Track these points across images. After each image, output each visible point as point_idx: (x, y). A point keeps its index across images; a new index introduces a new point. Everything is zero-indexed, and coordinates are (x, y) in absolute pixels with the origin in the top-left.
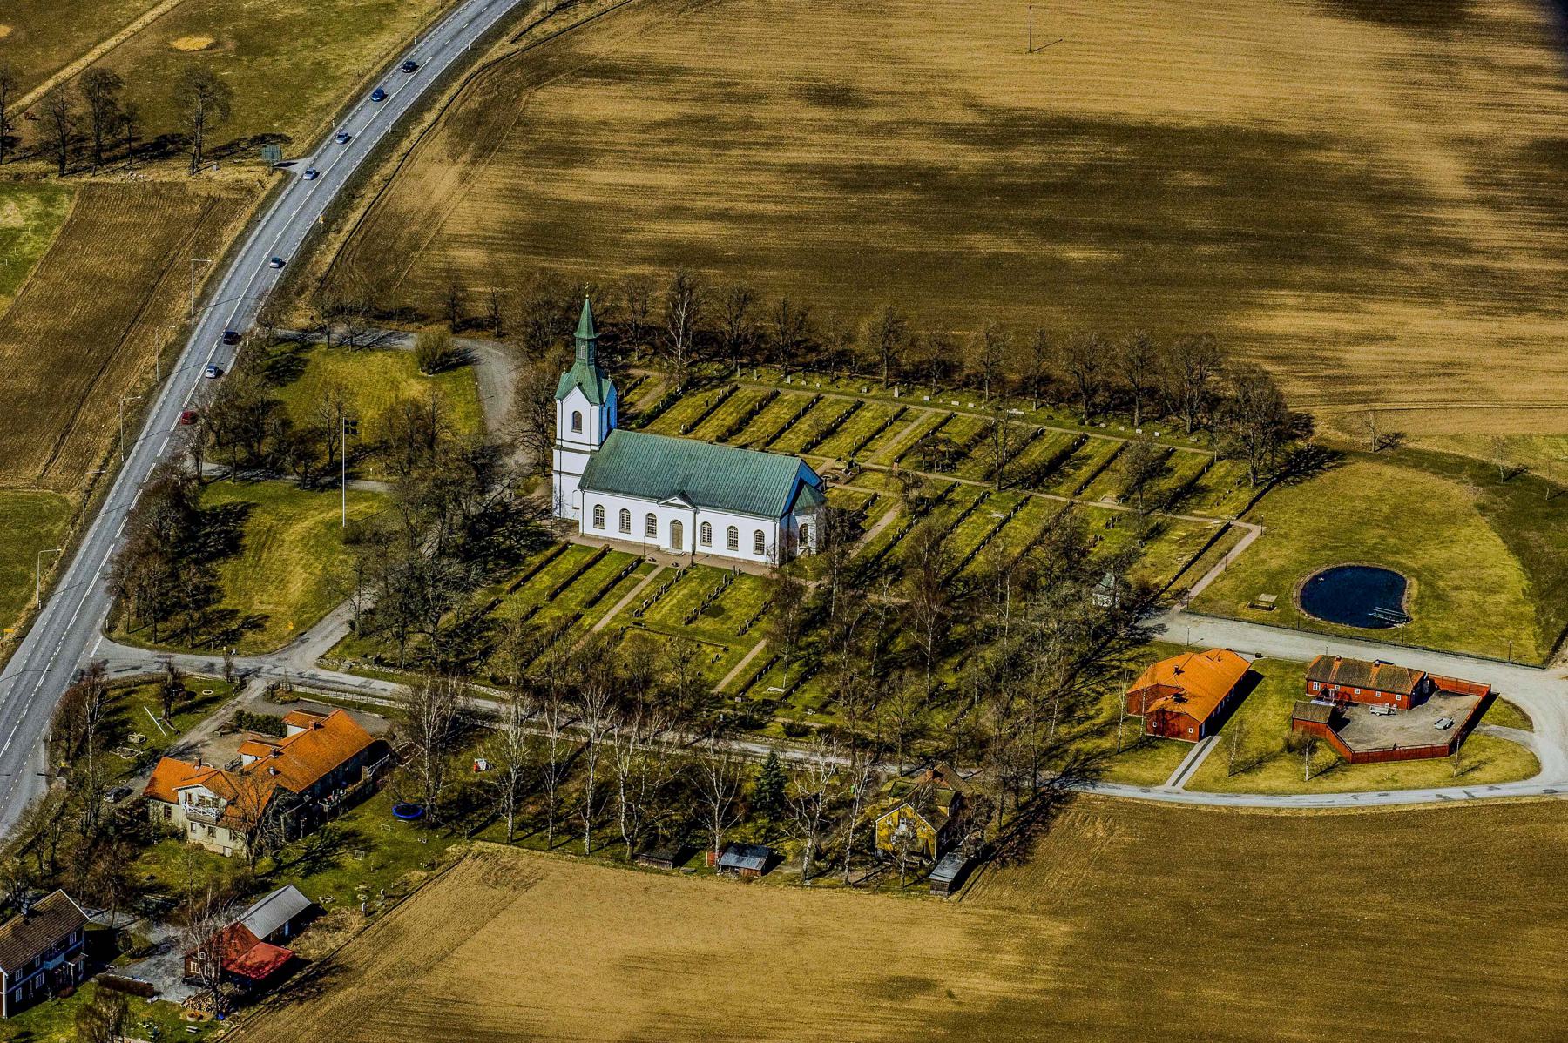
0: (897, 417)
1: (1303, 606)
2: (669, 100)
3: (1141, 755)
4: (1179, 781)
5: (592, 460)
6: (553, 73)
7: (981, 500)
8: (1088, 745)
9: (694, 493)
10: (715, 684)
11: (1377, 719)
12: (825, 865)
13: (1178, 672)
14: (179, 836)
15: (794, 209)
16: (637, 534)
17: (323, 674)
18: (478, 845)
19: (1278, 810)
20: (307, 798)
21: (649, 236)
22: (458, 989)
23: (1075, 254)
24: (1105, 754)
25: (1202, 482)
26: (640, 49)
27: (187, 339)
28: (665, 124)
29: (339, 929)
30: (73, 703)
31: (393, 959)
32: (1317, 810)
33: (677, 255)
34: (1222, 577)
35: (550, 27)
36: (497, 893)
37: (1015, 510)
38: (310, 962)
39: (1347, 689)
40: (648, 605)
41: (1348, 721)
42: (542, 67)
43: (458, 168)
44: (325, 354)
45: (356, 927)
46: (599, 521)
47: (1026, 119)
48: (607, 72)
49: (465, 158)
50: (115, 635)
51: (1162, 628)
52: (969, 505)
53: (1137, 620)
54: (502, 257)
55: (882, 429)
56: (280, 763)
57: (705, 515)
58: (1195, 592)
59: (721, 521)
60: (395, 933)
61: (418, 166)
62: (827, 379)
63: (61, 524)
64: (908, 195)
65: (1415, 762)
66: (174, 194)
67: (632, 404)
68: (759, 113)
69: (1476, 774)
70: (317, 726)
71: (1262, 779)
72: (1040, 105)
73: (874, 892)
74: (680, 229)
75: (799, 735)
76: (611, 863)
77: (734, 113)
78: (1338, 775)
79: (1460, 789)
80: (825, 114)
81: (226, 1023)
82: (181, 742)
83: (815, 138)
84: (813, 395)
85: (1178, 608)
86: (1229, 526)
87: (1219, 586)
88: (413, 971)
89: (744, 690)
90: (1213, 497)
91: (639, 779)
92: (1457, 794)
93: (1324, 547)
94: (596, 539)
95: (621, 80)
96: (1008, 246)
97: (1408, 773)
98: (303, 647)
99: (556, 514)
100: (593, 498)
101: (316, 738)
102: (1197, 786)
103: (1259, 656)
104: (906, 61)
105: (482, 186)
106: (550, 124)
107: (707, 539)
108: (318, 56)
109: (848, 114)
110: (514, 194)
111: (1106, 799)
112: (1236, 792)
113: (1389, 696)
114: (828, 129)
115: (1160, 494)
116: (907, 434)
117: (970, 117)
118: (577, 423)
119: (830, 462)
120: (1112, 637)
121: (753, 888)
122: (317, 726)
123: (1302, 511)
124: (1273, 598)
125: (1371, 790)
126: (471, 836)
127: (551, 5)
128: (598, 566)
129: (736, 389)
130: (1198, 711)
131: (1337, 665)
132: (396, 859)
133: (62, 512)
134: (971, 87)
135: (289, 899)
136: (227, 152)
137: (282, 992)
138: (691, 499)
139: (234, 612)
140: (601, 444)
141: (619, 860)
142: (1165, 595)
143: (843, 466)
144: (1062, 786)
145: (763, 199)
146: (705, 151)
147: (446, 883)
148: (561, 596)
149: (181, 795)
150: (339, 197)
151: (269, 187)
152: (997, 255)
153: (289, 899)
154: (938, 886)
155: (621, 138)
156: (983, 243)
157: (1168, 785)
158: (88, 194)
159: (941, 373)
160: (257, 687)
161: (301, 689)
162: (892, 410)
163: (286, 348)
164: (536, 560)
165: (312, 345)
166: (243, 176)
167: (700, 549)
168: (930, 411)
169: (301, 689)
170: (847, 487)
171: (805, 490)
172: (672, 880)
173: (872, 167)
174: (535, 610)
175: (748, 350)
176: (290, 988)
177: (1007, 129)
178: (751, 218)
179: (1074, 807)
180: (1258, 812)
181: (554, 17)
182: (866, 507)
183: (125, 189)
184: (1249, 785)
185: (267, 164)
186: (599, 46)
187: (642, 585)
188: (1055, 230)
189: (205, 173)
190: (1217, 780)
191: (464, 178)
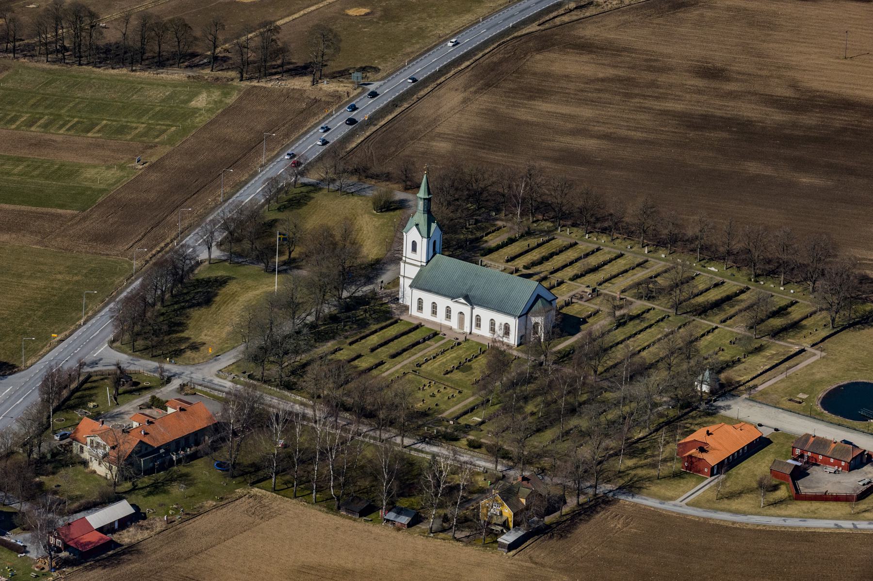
0: (639, 265)
1: (821, 403)
2: (613, 66)
3: (675, 482)
4: (685, 501)
5: (420, 271)
6: (553, 45)
7: (662, 320)
8: (641, 472)
9: (474, 297)
10: (443, 411)
11: (827, 475)
12: (444, 527)
13: (709, 434)
14: (85, 463)
15: (652, 136)
16: (440, 318)
17: (217, 380)
18: (255, 490)
19: (734, 523)
20: (162, 451)
21: (556, 144)
22: (197, 572)
23: (805, 180)
24: (650, 479)
25: (804, 323)
26: (612, 36)
27: (251, 179)
28: (603, 80)
29: (147, 529)
30: (45, 381)
31: (169, 550)
32: (758, 525)
33: (569, 157)
34: (782, 381)
35: (566, 18)
36: (251, 520)
37: (680, 327)
38: (122, 545)
39: (815, 456)
40: (427, 361)
41: (808, 474)
42: (545, 42)
43: (466, 94)
44: (325, 195)
45: (158, 529)
46: (420, 308)
47: (823, 97)
48: (585, 47)
49: (472, 89)
50: (115, 345)
51: (728, 407)
52: (653, 322)
53: (715, 401)
54: (460, 148)
55: (626, 271)
56: (150, 429)
57: (478, 311)
58: (760, 388)
59: (486, 315)
60: (180, 535)
61: (442, 91)
62: (610, 239)
63: (122, 278)
64: (725, 135)
65: (835, 503)
66: (296, 96)
67: (486, 241)
68: (663, 79)
69: (867, 514)
70: (182, 410)
71: (735, 504)
72: (835, 90)
73: (466, 545)
74: (576, 142)
75: (475, 447)
76: (325, 510)
77: (649, 76)
78: (783, 506)
79: (851, 522)
80: (700, 83)
81: (55, 574)
82: (118, 410)
83: (688, 96)
84: (596, 246)
85: (745, 396)
86: (803, 350)
87: (777, 385)
88: (179, 558)
89: (458, 418)
90: (805, 332)
91: (270, 461)
92: (847, 525)
93: (855, 369)
94: (417, 318)
95: (591, 52)
96: (768, 171)
97: (826, 509)
98: (215, 363)
99: (401, 301)
100: (418, 294)
101: (179, 416)
102: (694, 504)
103: (776, 430)
104: (768, 57)
105: (474, 107)
106: (535, 74)
107: (478, 325)
108: (423, 24)
109: (714, 84)
110: (490, 113)
111: (636, 504)
112: (716, 510)
113: (838, 462)
114: (700, 92)
115: (778, 324)
116: (641, 275)
117: (789, 93)
118: (414, 249)
119: (583, 288)
120: (695, 409)
121: (400, 535)
122: (182, 410)
123: (853, 346)
124: (805, 396)
125: (797, 517)
126: (253, 484)
127: (572, 5)
128: (410, 335)
129: (554, 239)
130: (712, 459)
131: (812, 439)
132: (203, 493)
133: (126, 271)
134: (798, 76)
135: (122, 509)
136: (341, 74)
137: (98, 561)
138: (470, 300)
139: (188, 339)
140: (428, 262)
141: (330, 509)
142: (741, 388)
143: (589, 290)
144: (614, 495)
145: (636, 129)
146: (618, 98)
147: (224, 510)
148: (379, 350)
149: (88, 440)
150: (387, 105)
151: (351, 96)
152: (758, 175)
153: (122, 509)
154: (502, 545)
155: (572, 86)
156: (753, 168)
157: (677, 502)
158: (249, 92)
159: (671, 242)
160: (176, 383)
161: (200, 388)
162: (640, 260)
163: (304, 189)
164: (374, 327)
165: (321, 189)
166: (340, 89)
167: (474, 331)
168: (663, 263)
169: (200, 388)
170: (586, 304)
171: (540, 301)
172: (356, 524)
173: (713, 116)
174: (359, 356)
175: (564, 216)
176: (104, 559)
177: (808, 101)
178: (625, 140)
179: (613, 508)
180: (722, 523)
181: (573, 13)
182: (589, 316)
183: (270, 91)
184: (728, 507)
185: (353, 83)
186: (589, 32)
187: (432, 348)
188: (800, 165)
189: (320, 85)
190: (708, 501)
191: (465, 101)
